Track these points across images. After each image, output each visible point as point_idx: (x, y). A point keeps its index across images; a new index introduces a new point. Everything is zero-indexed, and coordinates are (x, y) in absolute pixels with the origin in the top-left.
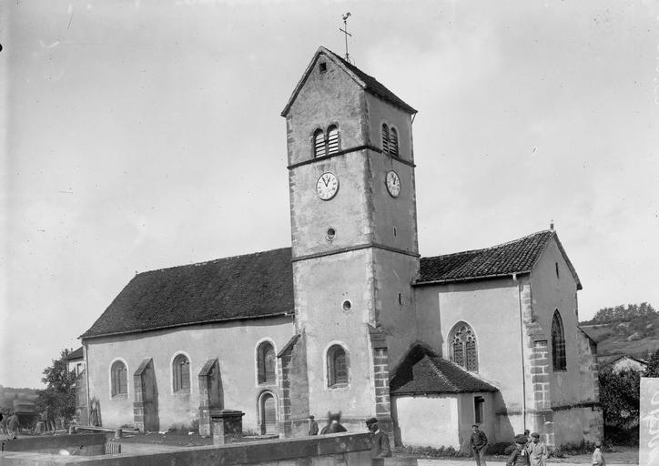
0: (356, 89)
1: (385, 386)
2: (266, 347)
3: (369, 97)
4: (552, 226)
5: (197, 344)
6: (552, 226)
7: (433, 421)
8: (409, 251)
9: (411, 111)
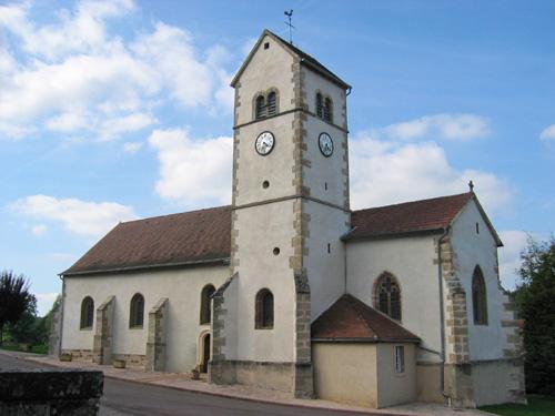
0: (288, 61)
1: (307, 331)
2: (209, 290)
3: (305, 70)
4: (471, 186)
5: (155, 289)
6: (471, 186)
7: (354, 369)
8: (346, 208)
9: (344, 87)
